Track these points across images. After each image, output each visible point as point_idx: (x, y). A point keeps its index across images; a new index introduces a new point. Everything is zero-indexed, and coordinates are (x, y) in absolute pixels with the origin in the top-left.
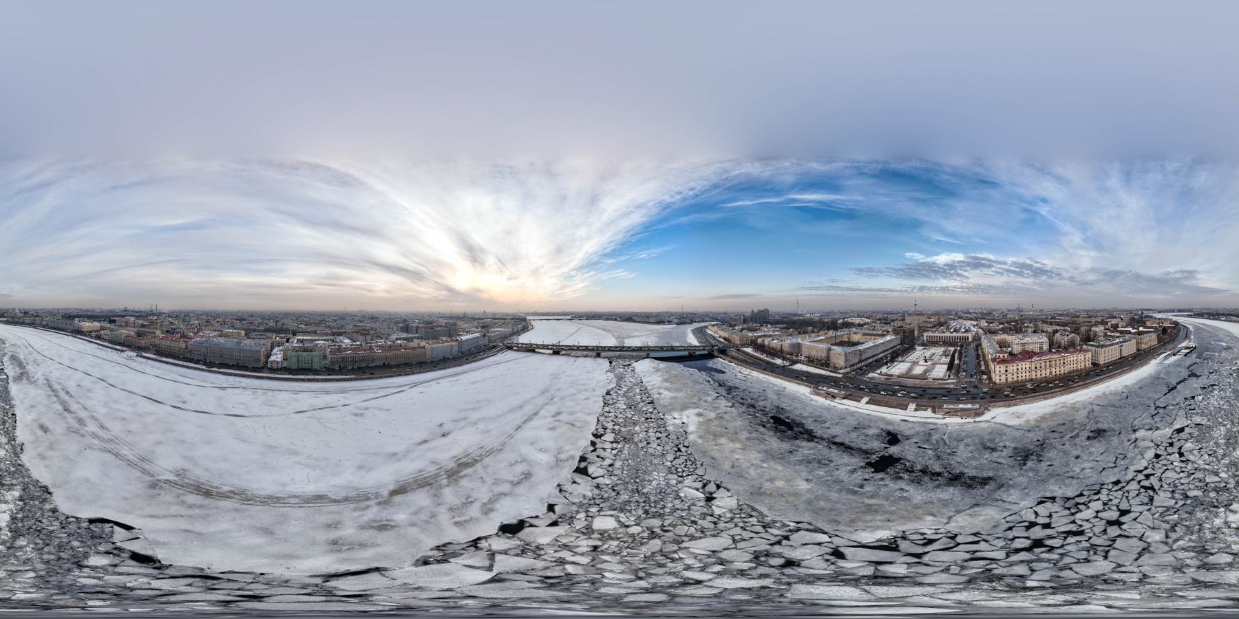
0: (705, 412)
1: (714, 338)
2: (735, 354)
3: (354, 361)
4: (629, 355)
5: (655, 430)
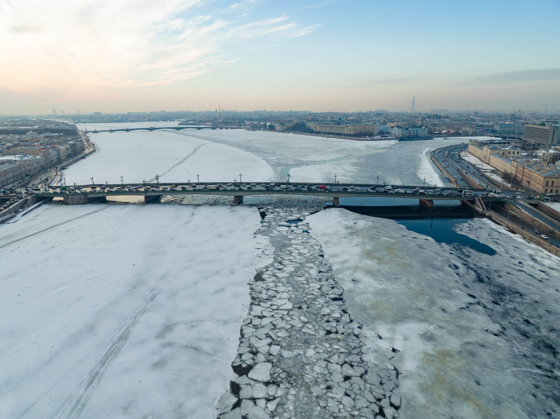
0: (439, 332)
1: (480, 174)
2: (525, 213)
4: (299, 201)
5: (343, 358)
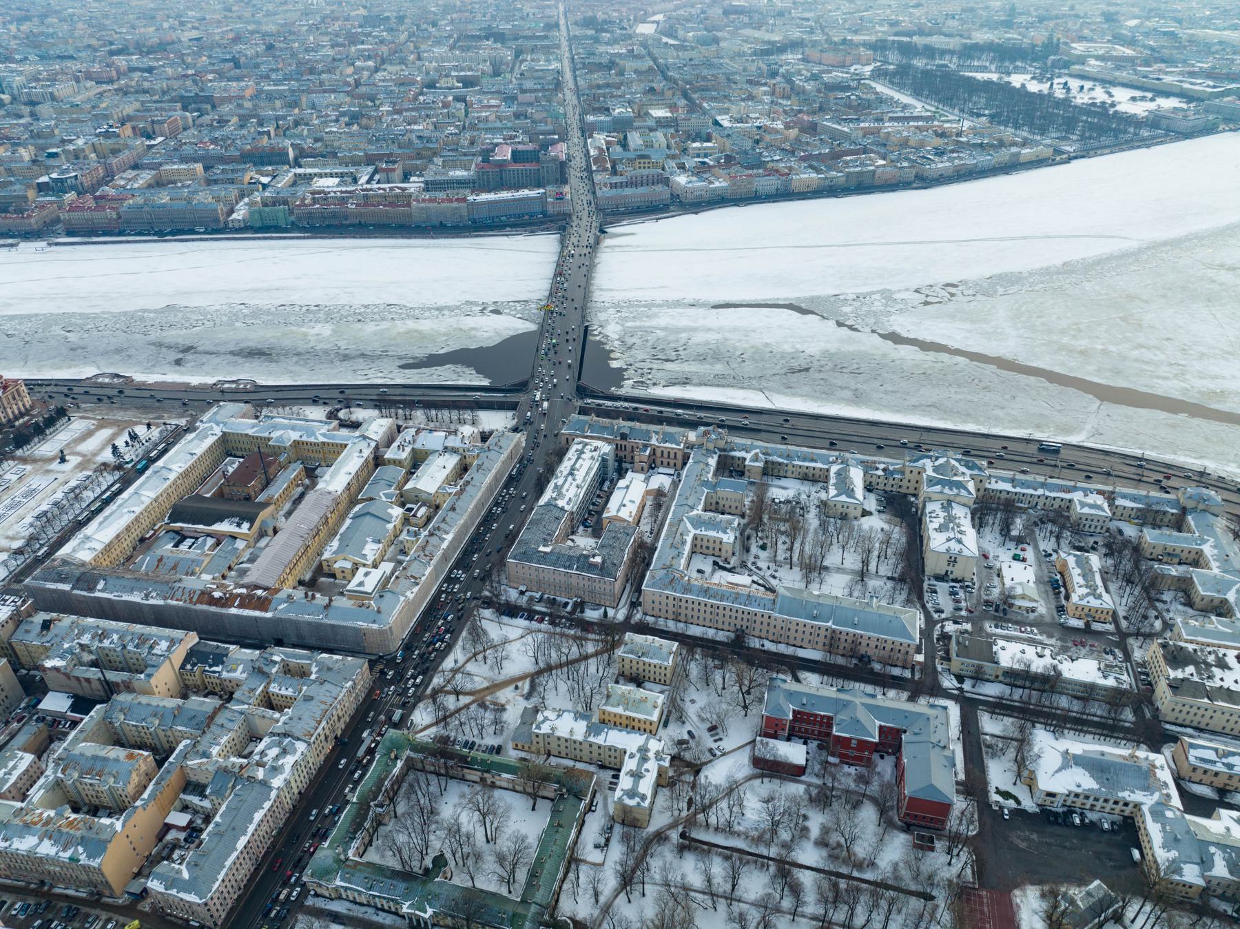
3: (323, 217)
